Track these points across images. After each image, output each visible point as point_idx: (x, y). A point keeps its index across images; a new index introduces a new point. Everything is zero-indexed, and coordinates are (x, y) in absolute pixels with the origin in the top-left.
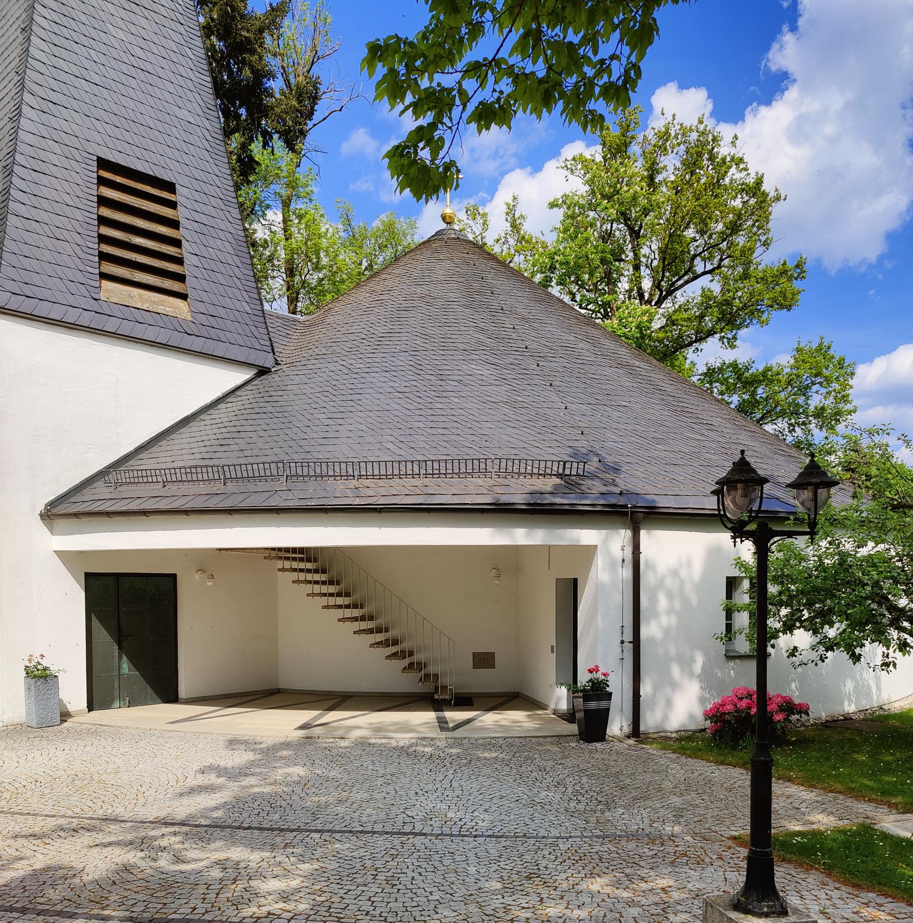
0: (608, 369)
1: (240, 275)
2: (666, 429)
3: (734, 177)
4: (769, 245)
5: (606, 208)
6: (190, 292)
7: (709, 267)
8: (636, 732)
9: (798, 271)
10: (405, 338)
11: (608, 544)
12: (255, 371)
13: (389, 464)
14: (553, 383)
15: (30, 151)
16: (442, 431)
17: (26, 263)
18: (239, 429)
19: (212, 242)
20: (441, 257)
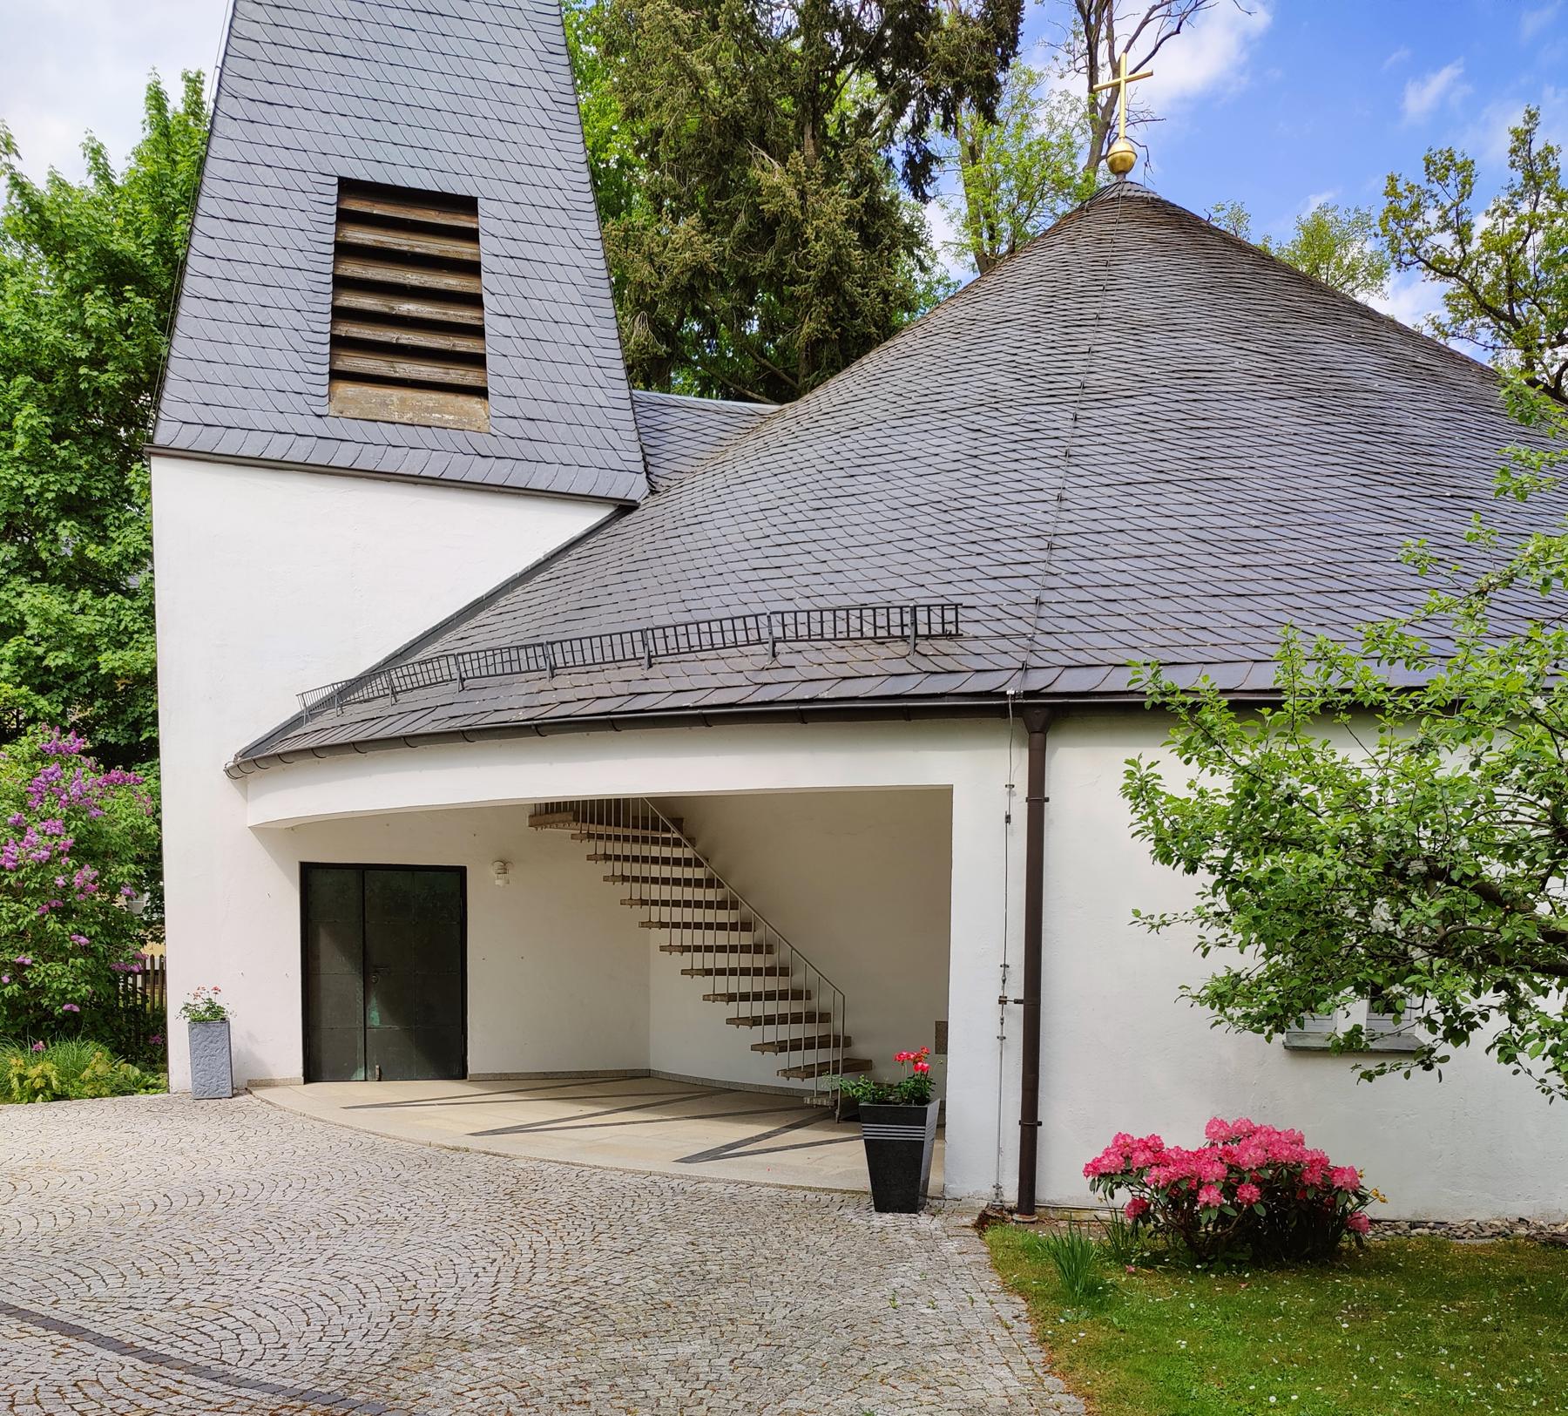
11: (976, 778)
15: (227, 190)
17: (208, 371)
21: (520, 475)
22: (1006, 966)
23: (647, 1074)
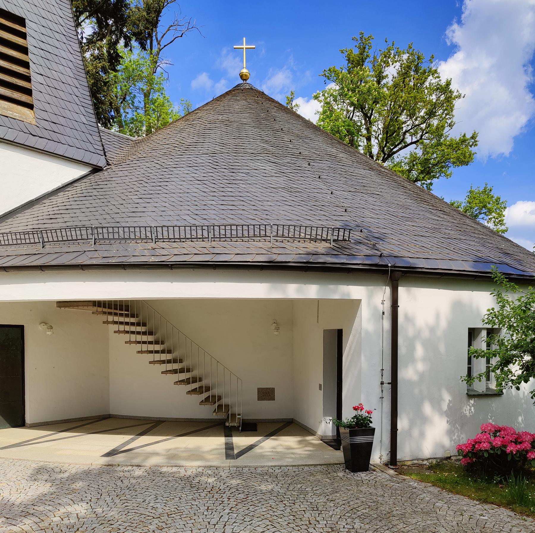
0: (363, 170)
1: (78, 94)
2: (411, 211)
3: (432, 82)
4: (452, 126)
5: (351, 97)
6: (35, 103)
7: (414, 140)
8: (393, 461)
9: (473, 141)
10: (207, 146)
11: (369, 299)
12: (90, 169)
13: (182, 229)
14: (321, 177)
16: (231, 207)
18: (67, 207)
19: (55, 66)
20: (238, 98)
21: (51, 147)
22: (383, 370)
23: (109, 417)
